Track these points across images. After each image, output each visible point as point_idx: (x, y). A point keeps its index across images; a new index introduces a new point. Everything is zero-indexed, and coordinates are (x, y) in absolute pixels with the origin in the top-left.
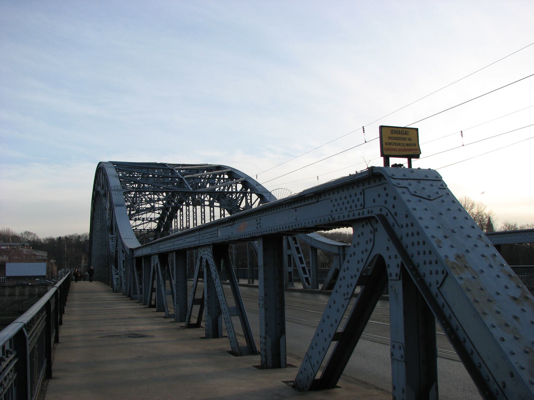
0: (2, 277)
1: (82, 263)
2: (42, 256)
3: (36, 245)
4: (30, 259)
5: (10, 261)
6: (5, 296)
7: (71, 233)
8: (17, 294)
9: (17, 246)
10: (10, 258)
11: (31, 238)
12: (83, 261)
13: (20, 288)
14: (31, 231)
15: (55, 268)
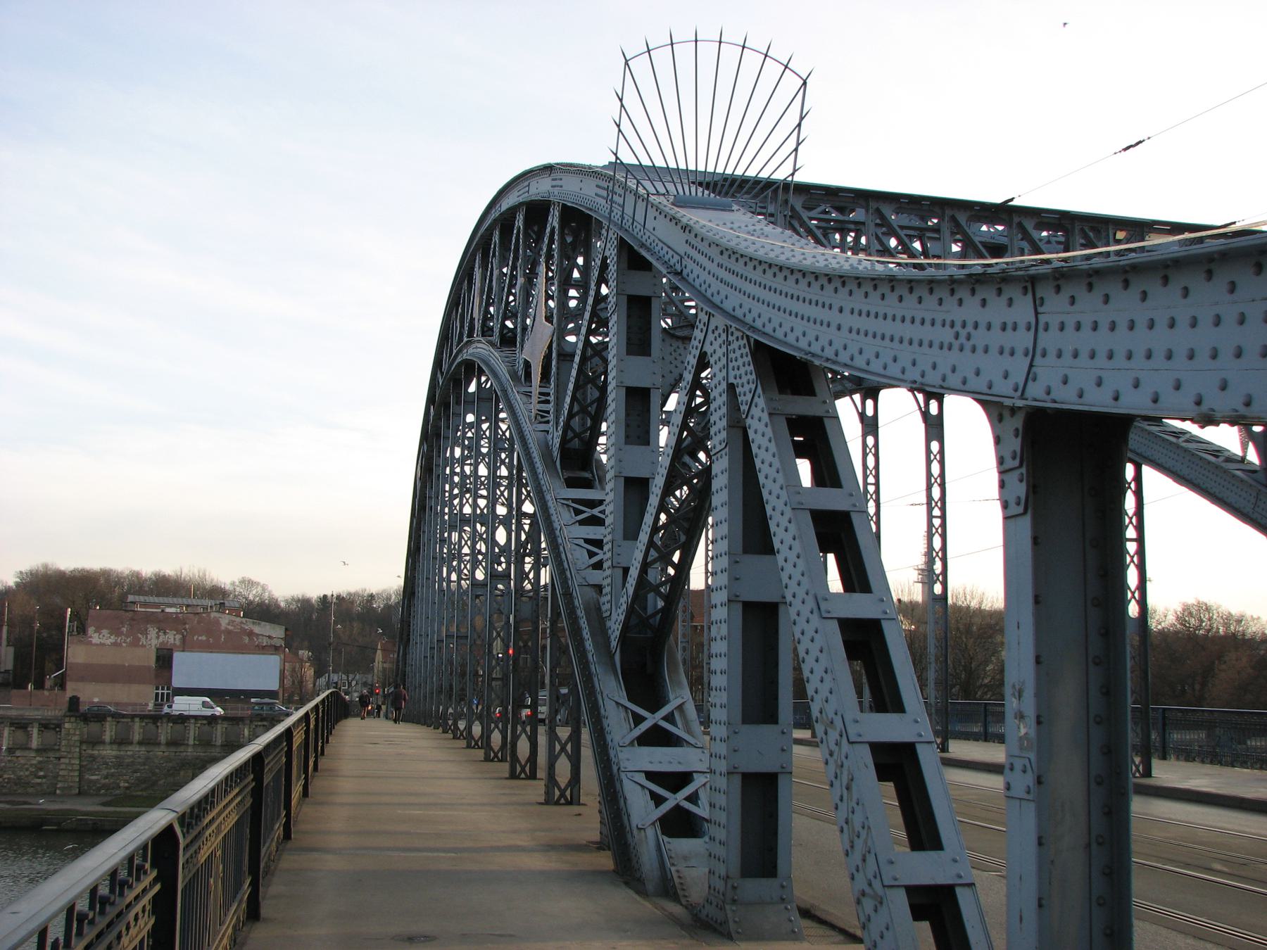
0: (163, 689)
1: (376, 661)
2: (270, 637)
3: (264, 611)
4: (237, 644)
5: (185, 646)
6: (159, 744)
7: (352, 589)
8: (191, 742)
9: (205, 608)
10: (184, 639)
11: (255, 596)
12: (379, 655)
13: (199, 725)
14: (255, 578)
15: (309, 672)
